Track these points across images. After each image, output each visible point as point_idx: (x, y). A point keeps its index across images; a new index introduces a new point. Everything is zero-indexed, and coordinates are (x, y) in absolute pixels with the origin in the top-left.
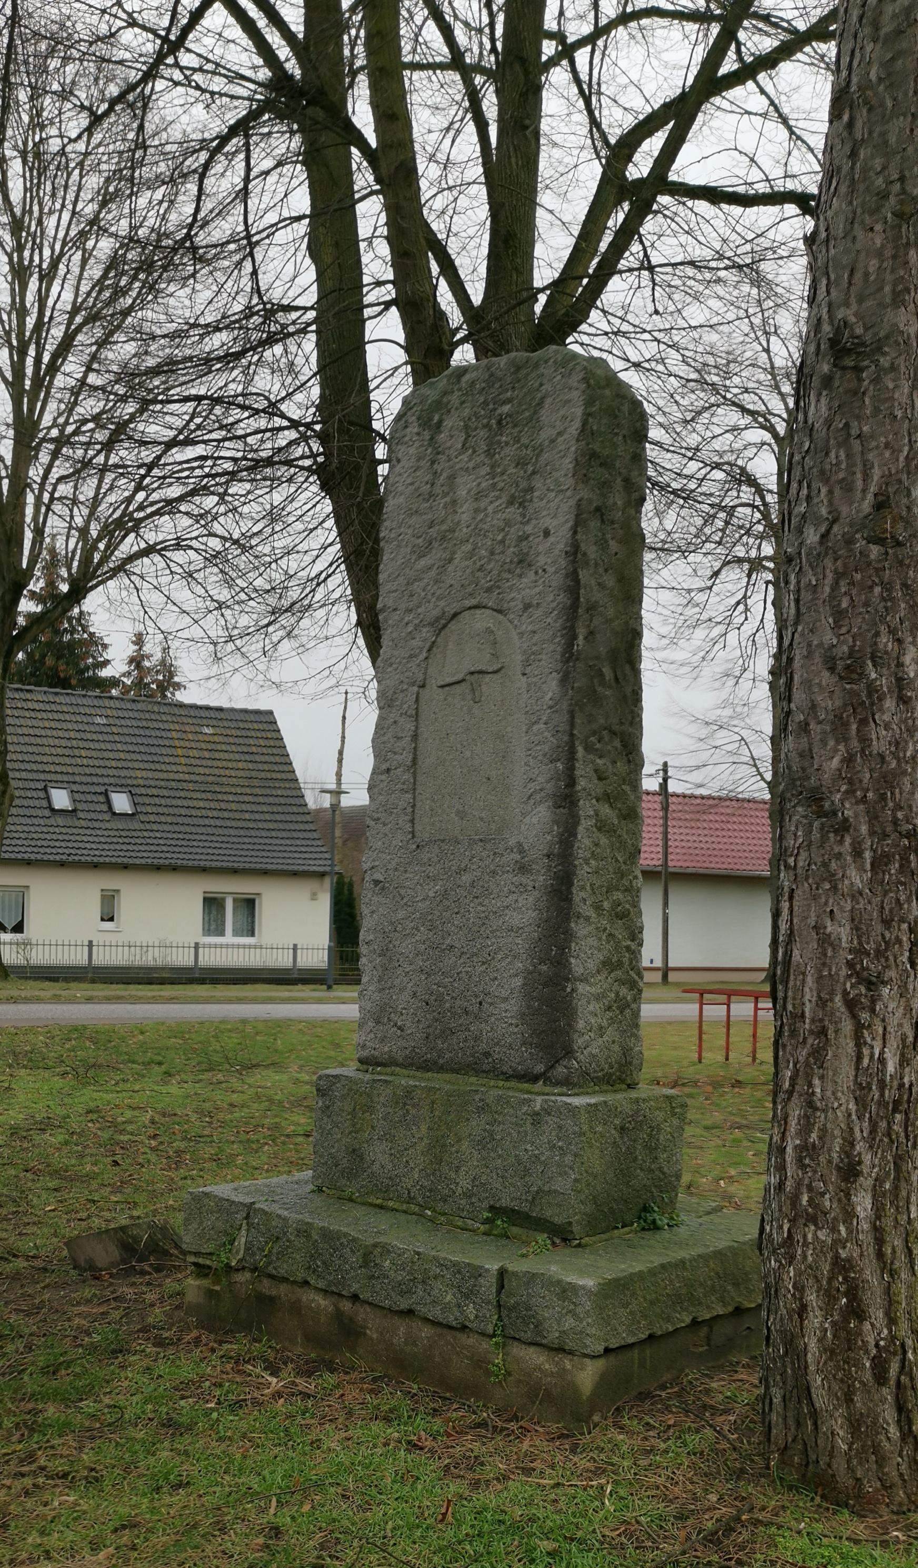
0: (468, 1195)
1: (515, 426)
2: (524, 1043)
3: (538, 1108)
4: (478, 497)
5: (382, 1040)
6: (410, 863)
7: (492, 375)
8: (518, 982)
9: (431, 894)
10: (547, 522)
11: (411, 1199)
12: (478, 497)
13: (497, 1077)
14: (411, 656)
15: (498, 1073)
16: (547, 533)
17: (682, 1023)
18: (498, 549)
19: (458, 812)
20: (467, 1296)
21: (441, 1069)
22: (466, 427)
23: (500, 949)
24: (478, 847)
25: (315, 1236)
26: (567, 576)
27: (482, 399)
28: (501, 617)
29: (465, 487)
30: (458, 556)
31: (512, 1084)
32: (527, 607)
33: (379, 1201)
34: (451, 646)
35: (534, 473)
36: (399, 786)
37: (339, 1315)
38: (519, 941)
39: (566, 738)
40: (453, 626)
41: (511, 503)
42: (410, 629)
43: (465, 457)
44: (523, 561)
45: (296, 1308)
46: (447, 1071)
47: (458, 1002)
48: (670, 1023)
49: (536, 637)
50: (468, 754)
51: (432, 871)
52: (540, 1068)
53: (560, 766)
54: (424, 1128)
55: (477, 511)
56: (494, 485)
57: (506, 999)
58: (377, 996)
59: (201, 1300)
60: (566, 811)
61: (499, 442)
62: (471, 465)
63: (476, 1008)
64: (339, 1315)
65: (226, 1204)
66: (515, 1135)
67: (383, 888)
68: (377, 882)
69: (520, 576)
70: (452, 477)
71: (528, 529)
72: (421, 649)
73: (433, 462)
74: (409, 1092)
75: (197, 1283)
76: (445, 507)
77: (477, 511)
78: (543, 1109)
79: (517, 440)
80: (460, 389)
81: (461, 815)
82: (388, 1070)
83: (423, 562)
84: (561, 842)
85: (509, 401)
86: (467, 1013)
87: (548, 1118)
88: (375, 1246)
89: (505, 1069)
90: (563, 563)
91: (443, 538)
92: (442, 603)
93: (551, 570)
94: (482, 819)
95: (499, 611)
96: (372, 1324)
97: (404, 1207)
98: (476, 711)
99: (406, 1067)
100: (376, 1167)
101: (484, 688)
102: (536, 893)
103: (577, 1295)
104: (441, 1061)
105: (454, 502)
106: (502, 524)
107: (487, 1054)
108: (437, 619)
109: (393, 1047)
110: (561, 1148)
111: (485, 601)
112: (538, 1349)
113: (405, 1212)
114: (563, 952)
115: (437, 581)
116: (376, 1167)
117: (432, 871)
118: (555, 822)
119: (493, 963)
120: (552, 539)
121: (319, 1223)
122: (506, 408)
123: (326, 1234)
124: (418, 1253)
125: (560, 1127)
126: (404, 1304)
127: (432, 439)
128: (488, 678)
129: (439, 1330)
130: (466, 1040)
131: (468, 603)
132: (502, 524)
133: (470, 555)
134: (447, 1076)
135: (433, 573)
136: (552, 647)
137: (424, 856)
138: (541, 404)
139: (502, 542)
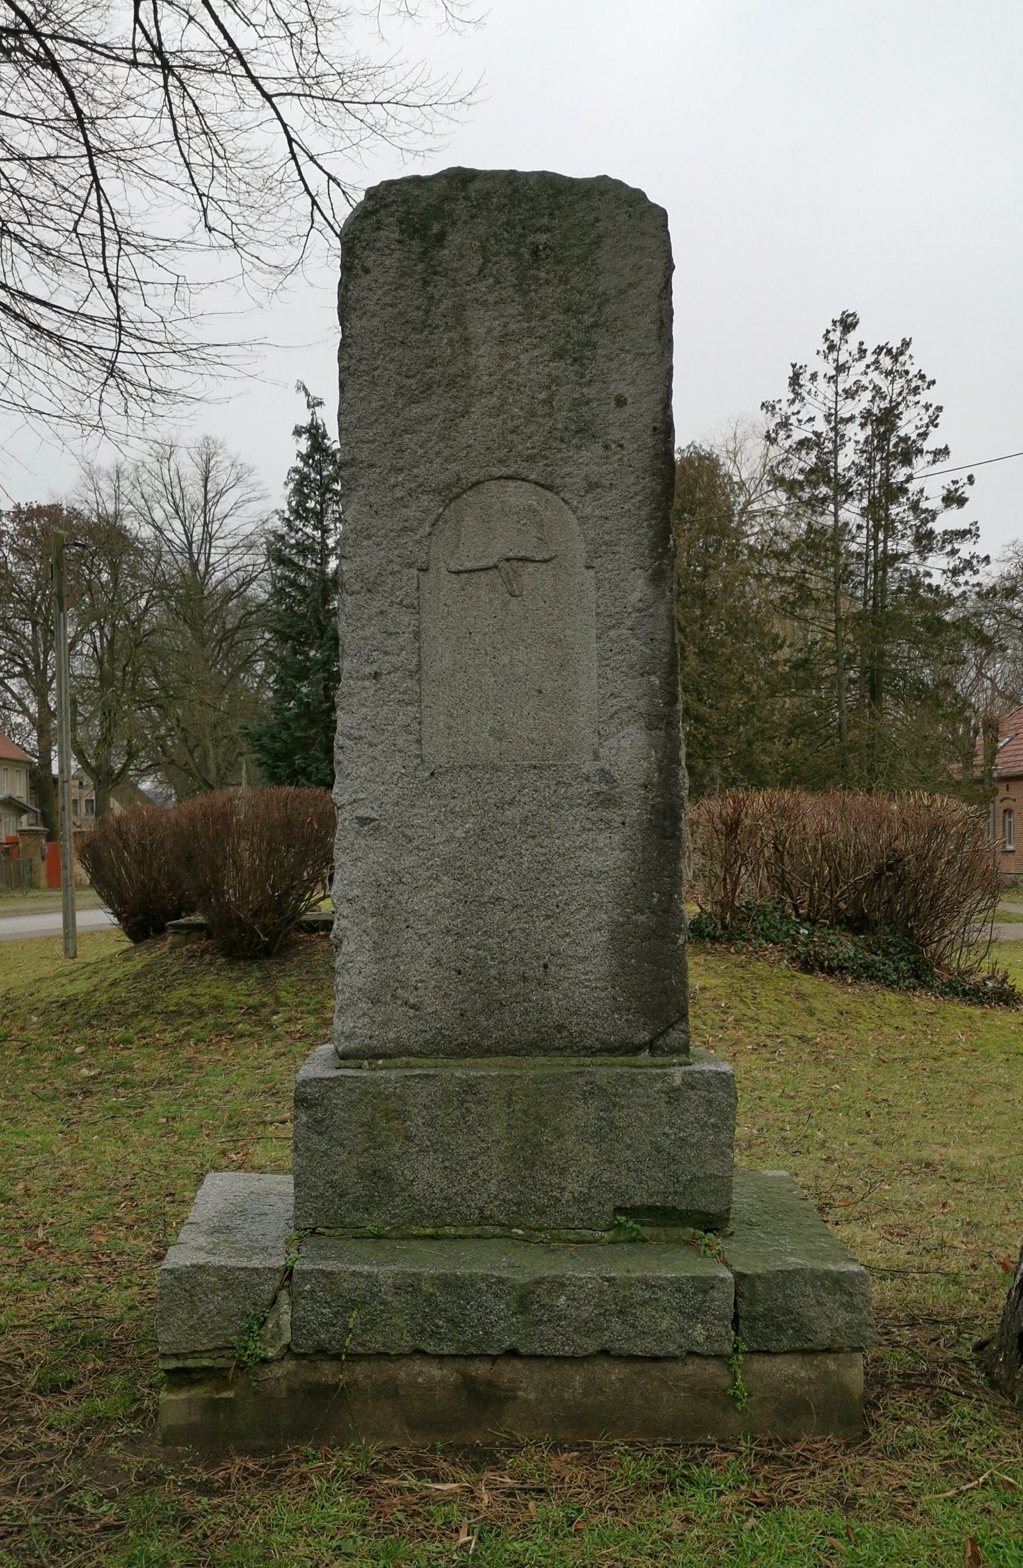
0: (580, 1200)
1: (559, 262)
2: (618, 1010)
3: (678, 1081)
4: (504, 339)
5: (384, 1024)
6: (420, 795)
7: (516, 191)
8: (601, 937)
9: (459, 834)
10: (622, 389)
11: (484, 1219)
12: (504, 339)
13: (576, 1053)
14: (405, 529)
15: (576, 1048)
16: (621, 402)
17: (48, 939)
18: (540, 410)
19: (492, 731)
20: (690, 1317)
21: (487, 1052)
22: (484, 249)
23: (573, 898)
24: (532, 775)
25: (426, 1287)
26: (656, 456)
27: (504, 218)
28: (549, 494)
29: (480, 324)
30: (476, 410)
31: (599, 1060)
32: (592, 487)
33: (429, 1231)
34: (468, 521)
35: (595, 325)
36: (395, 696)
37: (468, 1383)
38: (601, 887)
39: (665, 648)
40: (469, 497)
41: (559, 355)
42: (399, 493)
43: (482, 287)
44: (585, 431)
45: (389, 1391)
46: (497, 1054)
47: (511, 967)
48: (31, 940)
49: (609, 525)
50: (505, 659)
51: (458, 805)
52: (644, 1036)
53: (655, 680)
54: (498, 1130)
55: (504, 357)
56: (530, 331)
57: (582, 960)
58: (371, 969)
59: (196, 1418)
60: (662, 733)
61: (536, 279)
62: (491, 298)
63: (539, 973)
64: (468, 1383)
65: (243, 1275)
66: (646, 1119)
67: (377, 829)
68: (363, 821)
69: (578, 448)
70: (459, 308)
71: (590, 392)
72: (421, 522)
73: (426, 283)
74: (470, 1088)
75: (183, 1395)
76: (451, 343)
77: (504, 357)
78: (684, 1082)
79: (564, 280)
80: (467, 198)
81: (499, 735)
82: (398, 1061)
83: (416, 410)
84: (660, 770)
85: (548, 229)
86: (525, 979)
87: (691, 1094)
88: (539, 1282)
89: (588, 1043)
90: (650, 442)
91: (451, 383)
92: (455, 467)
93: (632, 447)
94: (532, 741)
95: (549, 488)
96: (527, 1382)
97: (477, 1230)
98: (513, 604)
99: (426, 1056)
100: (417, 1189)
101: (526, 579)
102: (627, 830)
103: (853, 1283)
104: (486, 1043)
105: (466, 340)
106: (546, 381)
107: (560, 1028)
108: (448, 486)
109: (403, 1030)
110: (713, 1125)
111: (525, 473)
112: (788, 1357)
113: (479, 1237)
114: (671, 899)
115: (442, 438)
116: (417, 1189)
117: (458, 805)
118: (652, 746)
119: (563, 916)
120: (628, 410)
121: (428, 1271)
122: (543, 238)
123: (447, 1283)
124: (609, 1280)
125: (710, 1102)
126: (591, 1346)
127: (425, 253)
128: (531, 567)
129: (638, 1367)
130: (526, 1012)
131: (495, 471)
132: (546, 381)
133: (497, 411)
134: (501, 1060)
135: (436, 424)
136: (635, 539)
137: (444, 785)
138: (598, 242)
139: (548, 402)
